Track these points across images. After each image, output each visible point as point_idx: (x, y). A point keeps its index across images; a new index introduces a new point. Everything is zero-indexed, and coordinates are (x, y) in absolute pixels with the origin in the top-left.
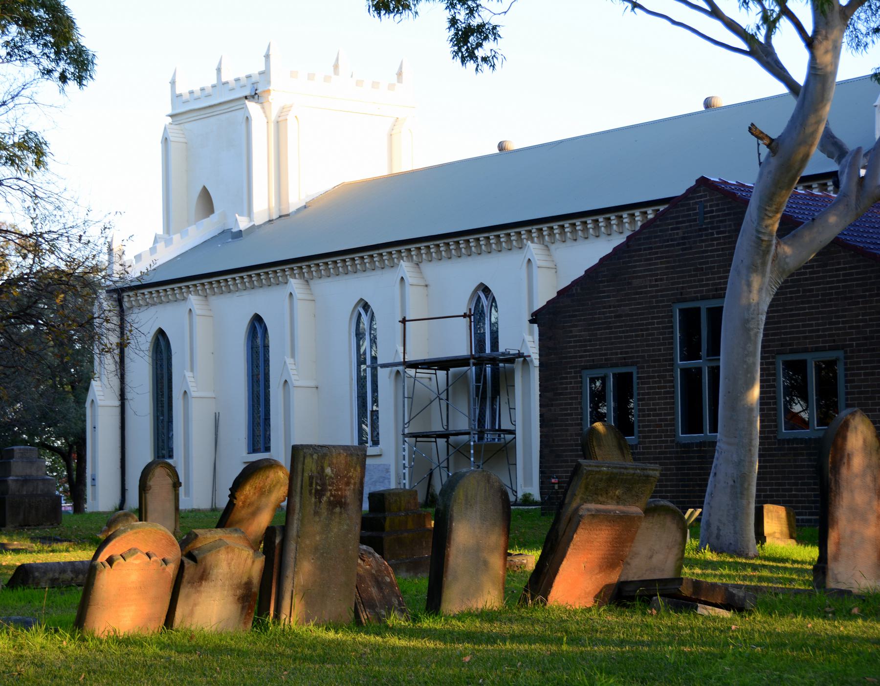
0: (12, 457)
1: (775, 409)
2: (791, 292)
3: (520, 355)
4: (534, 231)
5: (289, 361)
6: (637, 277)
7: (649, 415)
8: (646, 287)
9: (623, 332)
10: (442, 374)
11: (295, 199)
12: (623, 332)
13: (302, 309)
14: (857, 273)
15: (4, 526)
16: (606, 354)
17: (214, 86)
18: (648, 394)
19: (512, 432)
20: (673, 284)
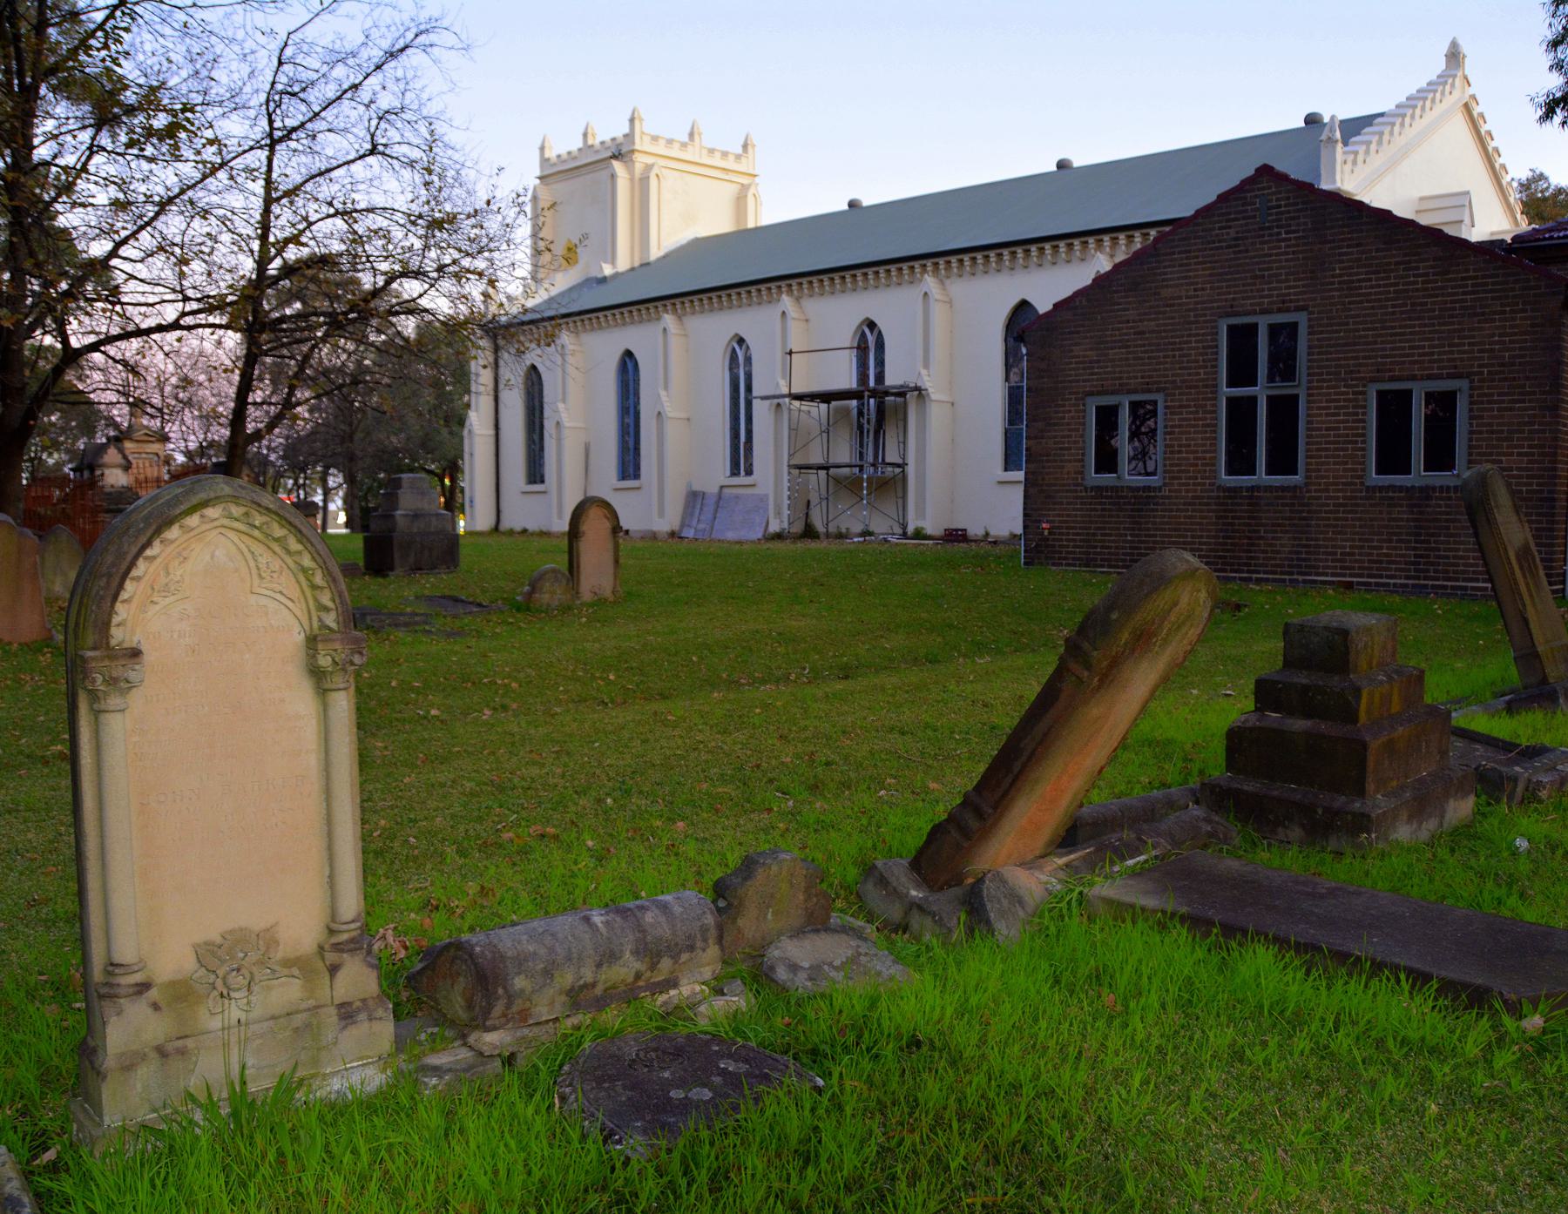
0: (400, 487)
1: (1363, 449)
2: (1394, 306)
3: (917, 389)
4: (929, 264)
5: (663, 393)
6: (1167, 286)
7: (1180, 452)
8: (1181, 298)
9: (1145, 352)
10: (824, 406)
11: (655, 253)
12: (1145, 352)
13: (675, 343)
14: (1493, 284)
15: (392, 569)
16: (1121, 378)
17: (580, 150)
18: (1180, 426)
19: (903, 466)
20: (1219, 294)
